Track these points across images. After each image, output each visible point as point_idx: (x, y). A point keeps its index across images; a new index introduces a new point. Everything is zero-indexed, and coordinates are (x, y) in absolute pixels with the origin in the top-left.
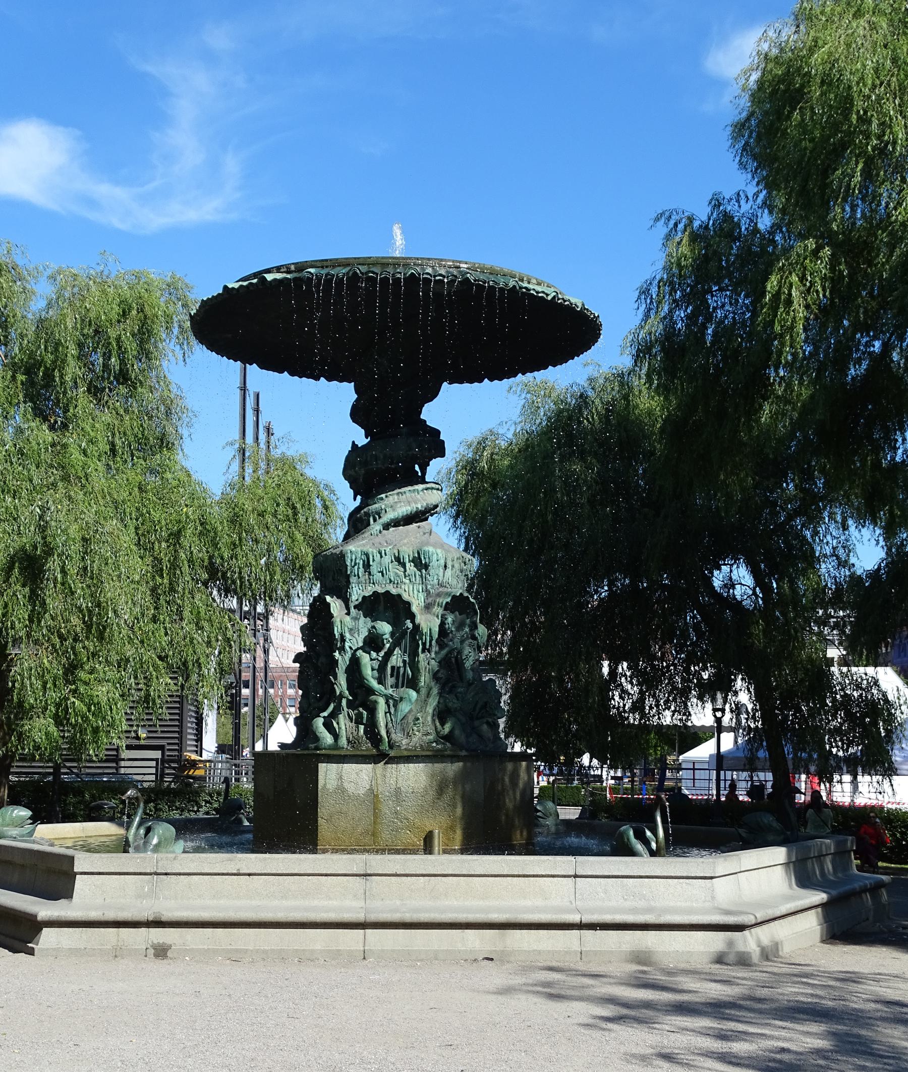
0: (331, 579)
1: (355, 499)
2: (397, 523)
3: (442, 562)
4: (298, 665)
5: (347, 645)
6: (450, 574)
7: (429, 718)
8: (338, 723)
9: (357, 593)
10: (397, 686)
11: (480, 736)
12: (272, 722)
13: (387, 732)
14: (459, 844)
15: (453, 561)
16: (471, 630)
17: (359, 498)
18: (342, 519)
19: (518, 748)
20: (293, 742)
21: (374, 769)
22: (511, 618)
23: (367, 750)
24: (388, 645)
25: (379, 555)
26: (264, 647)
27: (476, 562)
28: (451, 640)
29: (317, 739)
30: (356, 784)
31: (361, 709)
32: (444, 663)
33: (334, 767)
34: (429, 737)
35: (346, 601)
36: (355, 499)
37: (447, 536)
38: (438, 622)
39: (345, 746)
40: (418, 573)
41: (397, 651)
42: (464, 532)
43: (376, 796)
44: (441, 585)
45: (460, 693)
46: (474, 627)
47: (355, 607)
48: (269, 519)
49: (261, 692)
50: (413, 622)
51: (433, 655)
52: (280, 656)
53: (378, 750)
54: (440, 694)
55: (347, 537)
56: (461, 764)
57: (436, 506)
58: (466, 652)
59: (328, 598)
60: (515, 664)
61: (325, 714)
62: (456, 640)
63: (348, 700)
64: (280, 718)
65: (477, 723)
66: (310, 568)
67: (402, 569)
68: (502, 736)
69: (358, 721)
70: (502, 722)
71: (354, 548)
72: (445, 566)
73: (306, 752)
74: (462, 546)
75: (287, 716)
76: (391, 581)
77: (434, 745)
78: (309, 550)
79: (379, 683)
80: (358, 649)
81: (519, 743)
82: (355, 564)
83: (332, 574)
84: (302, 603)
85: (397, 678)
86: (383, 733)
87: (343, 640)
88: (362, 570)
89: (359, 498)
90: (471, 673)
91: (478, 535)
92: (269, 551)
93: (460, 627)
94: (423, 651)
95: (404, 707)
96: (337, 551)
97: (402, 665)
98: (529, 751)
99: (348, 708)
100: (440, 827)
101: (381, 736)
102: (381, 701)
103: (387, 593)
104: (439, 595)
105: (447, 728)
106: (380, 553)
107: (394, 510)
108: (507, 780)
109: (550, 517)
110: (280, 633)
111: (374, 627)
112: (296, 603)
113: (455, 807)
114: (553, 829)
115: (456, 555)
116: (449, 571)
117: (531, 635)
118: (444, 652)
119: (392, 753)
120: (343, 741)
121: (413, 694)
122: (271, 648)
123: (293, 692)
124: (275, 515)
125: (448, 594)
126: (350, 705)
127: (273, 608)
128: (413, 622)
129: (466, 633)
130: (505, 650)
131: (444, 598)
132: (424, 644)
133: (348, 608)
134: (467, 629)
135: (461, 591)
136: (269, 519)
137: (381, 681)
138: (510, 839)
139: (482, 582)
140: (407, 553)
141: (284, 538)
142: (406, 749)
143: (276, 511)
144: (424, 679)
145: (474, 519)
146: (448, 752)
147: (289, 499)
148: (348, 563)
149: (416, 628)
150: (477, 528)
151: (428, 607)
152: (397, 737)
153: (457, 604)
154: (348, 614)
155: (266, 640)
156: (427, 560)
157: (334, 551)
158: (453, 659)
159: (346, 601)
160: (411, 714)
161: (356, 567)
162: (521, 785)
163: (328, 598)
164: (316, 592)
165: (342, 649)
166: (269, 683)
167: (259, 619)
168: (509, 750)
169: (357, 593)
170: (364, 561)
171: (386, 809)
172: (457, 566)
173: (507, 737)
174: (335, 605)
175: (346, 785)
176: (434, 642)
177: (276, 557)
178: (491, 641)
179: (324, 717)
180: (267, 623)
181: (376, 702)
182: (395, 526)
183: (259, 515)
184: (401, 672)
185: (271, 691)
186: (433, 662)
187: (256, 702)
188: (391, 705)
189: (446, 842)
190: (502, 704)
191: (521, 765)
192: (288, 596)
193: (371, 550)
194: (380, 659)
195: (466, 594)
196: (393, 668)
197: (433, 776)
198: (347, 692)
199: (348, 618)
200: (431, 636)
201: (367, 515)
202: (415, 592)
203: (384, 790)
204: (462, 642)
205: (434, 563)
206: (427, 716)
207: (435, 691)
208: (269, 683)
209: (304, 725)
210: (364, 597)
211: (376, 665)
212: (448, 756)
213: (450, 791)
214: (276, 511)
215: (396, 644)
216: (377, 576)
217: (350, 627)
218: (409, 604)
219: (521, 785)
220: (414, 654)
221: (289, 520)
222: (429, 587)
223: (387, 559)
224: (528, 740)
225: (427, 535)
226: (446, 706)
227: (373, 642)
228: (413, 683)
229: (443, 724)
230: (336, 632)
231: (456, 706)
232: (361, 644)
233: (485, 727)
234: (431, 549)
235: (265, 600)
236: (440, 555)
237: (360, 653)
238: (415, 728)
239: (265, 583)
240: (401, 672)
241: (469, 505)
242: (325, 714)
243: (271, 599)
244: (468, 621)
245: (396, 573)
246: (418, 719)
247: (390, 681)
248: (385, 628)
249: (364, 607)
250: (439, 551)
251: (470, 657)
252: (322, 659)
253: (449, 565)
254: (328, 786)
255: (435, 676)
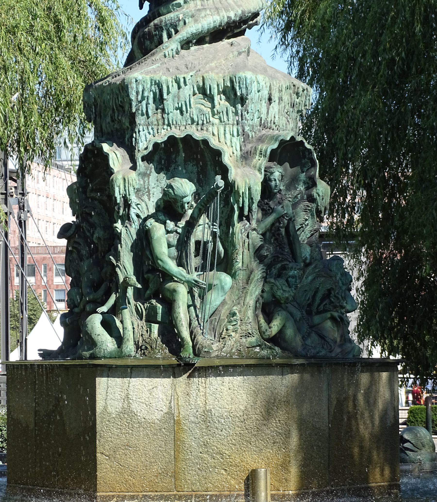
0: (109, 119)
1: (141, 7)
2: (200, 39)
3: (265, 93)
4: (64, 242)
5: (133, 212)
6: (276, 110)
7: (250, 313)
8: (122, 322)
9: (145, 140)
10: (203, 268)
11: (322, 337)
12: (32, 322)
13: (191, 333)
14: (293, 488)
15: (280, 91)
16: (307, 188)
17: (147, 4)
18: (124, 35)
19: (377, 353)
20: (60, 348)
21: (174, 387)
22: (364, 172)
23: (164, 358)
24: (190, 212)
25: (175, 85)
26: (19, 218)
27: (313, 94)
28: (280, 203)
29: (92, 343)
30: (149, 405)
31: (154, 301)
32: (271, 234)
33: (116, 383)
34: (249, 339)
35: (131, 150)
36: (141, 7)
37: (273, 57)
38: (260, 177)
39: (133, 354)
40: (231, 109)
41: (203, 220)
42: (298, 52)
43: (177, 423)
44: (263, 125)
45: (293, 277)
46: (311, 184)
47: (143, 159)
48: (22, 37)
49: (17, 281)
50: (225, 177)
51: (254, 224)
52: (42, 230)
53: (180, 358)
54: (265, 279)
55: (131, 60)
56: (295, 377)
57: (256, 15)
58: (300, 220)
59: (106, 147)
60: (372, 236)
61: (104, 309)
62: (286, 202)
63: (136, 290)
64: (44, 318)
65: (317, 319)
66: (79, 106)
67: (209, 105)
68: (354, 337)
69: (151, 318)
70: (353, 317)
71: (141, 77)
72: (270, 99)
73: (77, 362)
74: (295, 71)
75: (55, 314)
76: (193, 121)
77: (257, 349)
78: (80, 81)
79: (180, 264)
80: (148, 217)
81: (379, 348)
82: (143, 98)
83: (111, 113)
84: (70, 155)
85: (204, 258)
86: (185, 334)
87: (127, 205)
88: (152, 106)
89: (147, 4)
90: (308, 249)
91: (317, 55)
92: (23, 82)
93: (292, 183)
94: (240, 219)
95: (215, 299)
96: (117, 80)
97: (210, 239)
98: (391, 357)
99: (136, 300)
100: (268, 465)
101: (182, 339)
102: (182, 292)
103: (188, 139)
104: (261, 140)
105: (276, 326)
106: (177, 82)
107: (196, 21)
108: (360, 398)
109: (418, 28)
110: (42, 199)
111: (170, 186)
112: (64, 157)
113: (288, 435)
114: (427, 466)
115: (284, 84)
116: (275, 106)
117: (392, 196)
118: (270, 219)
119: (199, 362)
120: (129, 347)
121: (227, 279)
122: (30, 219)
123: (62, 281)
124: (30, 31)
125: (274, 138)
126: (139, 295)
127: (29, 162)
128: (225, 177)
129: (301, 192)
130: (356, 217)
131: (269, 143)
132: (241, 209)
133: (133, 159)
134: (301, 187)
135: (292, 134)
136: (22, 37)
137: (181, 262)
138: (366, 480)
139: (325, 120)
140: (216, 80)
141: (44, 64)
142: (217, 356)
143: (32, 26)
144: (242, 258)
145: (310, 33)
146: (278, 360)
147: (49, 9)
148: (133, 97)
149: (230, 187)
150: (316, 46)
151: (246, 157)
152: (205, 339)
153: (287, 152)
154: (134, 168)
155: (22, 208)
156: (244, 91)
157: (113, 81)
158: (283, 230)
159: (131, 150)
160: (226, 306)
161: (144, 103)
162: (380, 405)
163: (106, 147)
164: (89, 138)
165: (126, 218)
166: (28, 269)
167: (11, 178)
168: (365, 355)
169: (145, 140)
170: (155, 94)
171: (191, 440)
172: (286, 98)
173: (361, 339)
174: (116, 157)
175: (134, 406)
176: (255, 206)
177: (32, 91)
178: (336, 205)
179: (102, 313)
180: (23, 184)
181: (174, 291)
182: (394, 415)
183: (9, 31)
184: (210, 249)
185: (31, 280)
186: (254, 234)
187: (10, 296)
188: (196, 295)
189: (277, 484)
190: (353, 292)
191: (380, 377)
192: (51, 146)
193: (164, 78)
194: (180, 230)
195: (299, 138)
196: (198, 243)
197: (256, 393)
198: (134, 278)
199: (133, 175)
200: (251, 199)
201: (159, 28)
202: (228, 136)
203: (188, 412)
204: (295, 206)
205: (253, 96)
206: (246, 310)
207: (258, 274)
208: (28, 269)
209: (74, 324)
210: (156, 145)
211: (174, 239)
212: (277, 365)
213: (281, 415)
214: (32, 26)
215: (202, 209)
216: (174, 115)
217: (137, 186)
218: (218, 154)
219: (380, 405)
220: (227, 224)
221: (50, 39)
222: (247, 128)
223: (187, 91)
224: (391, 343)
225: (243, 56)
226: (274, 296)
227: (169, 208)
228: (226, 264)
229: (269, 321)
230: (117, 194)
231: (287, 295)
232: (152, 210)
233: (329, 324)
234: (249, 75)
235: (19, 151)
236: (262, 83)
237: (151, 223)
238: (230, 327)
239: (18, 128)
240: (210, 249)
241: (304, 12)
242: (104, 309)
243: (26, 150)
244: (303, 176)
245: (200, 110)
246: (234, 314)
247: (194, 261)
248: (185, 187)
249: (156, 158)
250: (260, 78)
251: (307, 227)
252: (98, 233)
253: (275, 97)
254: (110, 409)
255: (258, 254)
